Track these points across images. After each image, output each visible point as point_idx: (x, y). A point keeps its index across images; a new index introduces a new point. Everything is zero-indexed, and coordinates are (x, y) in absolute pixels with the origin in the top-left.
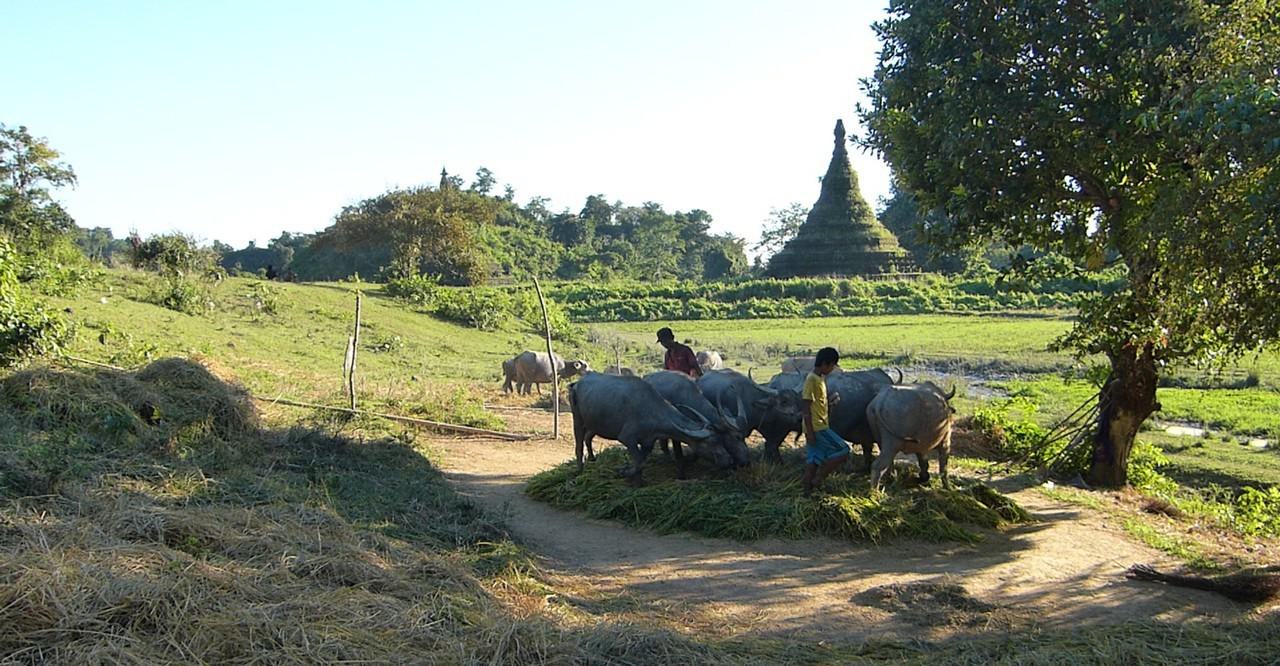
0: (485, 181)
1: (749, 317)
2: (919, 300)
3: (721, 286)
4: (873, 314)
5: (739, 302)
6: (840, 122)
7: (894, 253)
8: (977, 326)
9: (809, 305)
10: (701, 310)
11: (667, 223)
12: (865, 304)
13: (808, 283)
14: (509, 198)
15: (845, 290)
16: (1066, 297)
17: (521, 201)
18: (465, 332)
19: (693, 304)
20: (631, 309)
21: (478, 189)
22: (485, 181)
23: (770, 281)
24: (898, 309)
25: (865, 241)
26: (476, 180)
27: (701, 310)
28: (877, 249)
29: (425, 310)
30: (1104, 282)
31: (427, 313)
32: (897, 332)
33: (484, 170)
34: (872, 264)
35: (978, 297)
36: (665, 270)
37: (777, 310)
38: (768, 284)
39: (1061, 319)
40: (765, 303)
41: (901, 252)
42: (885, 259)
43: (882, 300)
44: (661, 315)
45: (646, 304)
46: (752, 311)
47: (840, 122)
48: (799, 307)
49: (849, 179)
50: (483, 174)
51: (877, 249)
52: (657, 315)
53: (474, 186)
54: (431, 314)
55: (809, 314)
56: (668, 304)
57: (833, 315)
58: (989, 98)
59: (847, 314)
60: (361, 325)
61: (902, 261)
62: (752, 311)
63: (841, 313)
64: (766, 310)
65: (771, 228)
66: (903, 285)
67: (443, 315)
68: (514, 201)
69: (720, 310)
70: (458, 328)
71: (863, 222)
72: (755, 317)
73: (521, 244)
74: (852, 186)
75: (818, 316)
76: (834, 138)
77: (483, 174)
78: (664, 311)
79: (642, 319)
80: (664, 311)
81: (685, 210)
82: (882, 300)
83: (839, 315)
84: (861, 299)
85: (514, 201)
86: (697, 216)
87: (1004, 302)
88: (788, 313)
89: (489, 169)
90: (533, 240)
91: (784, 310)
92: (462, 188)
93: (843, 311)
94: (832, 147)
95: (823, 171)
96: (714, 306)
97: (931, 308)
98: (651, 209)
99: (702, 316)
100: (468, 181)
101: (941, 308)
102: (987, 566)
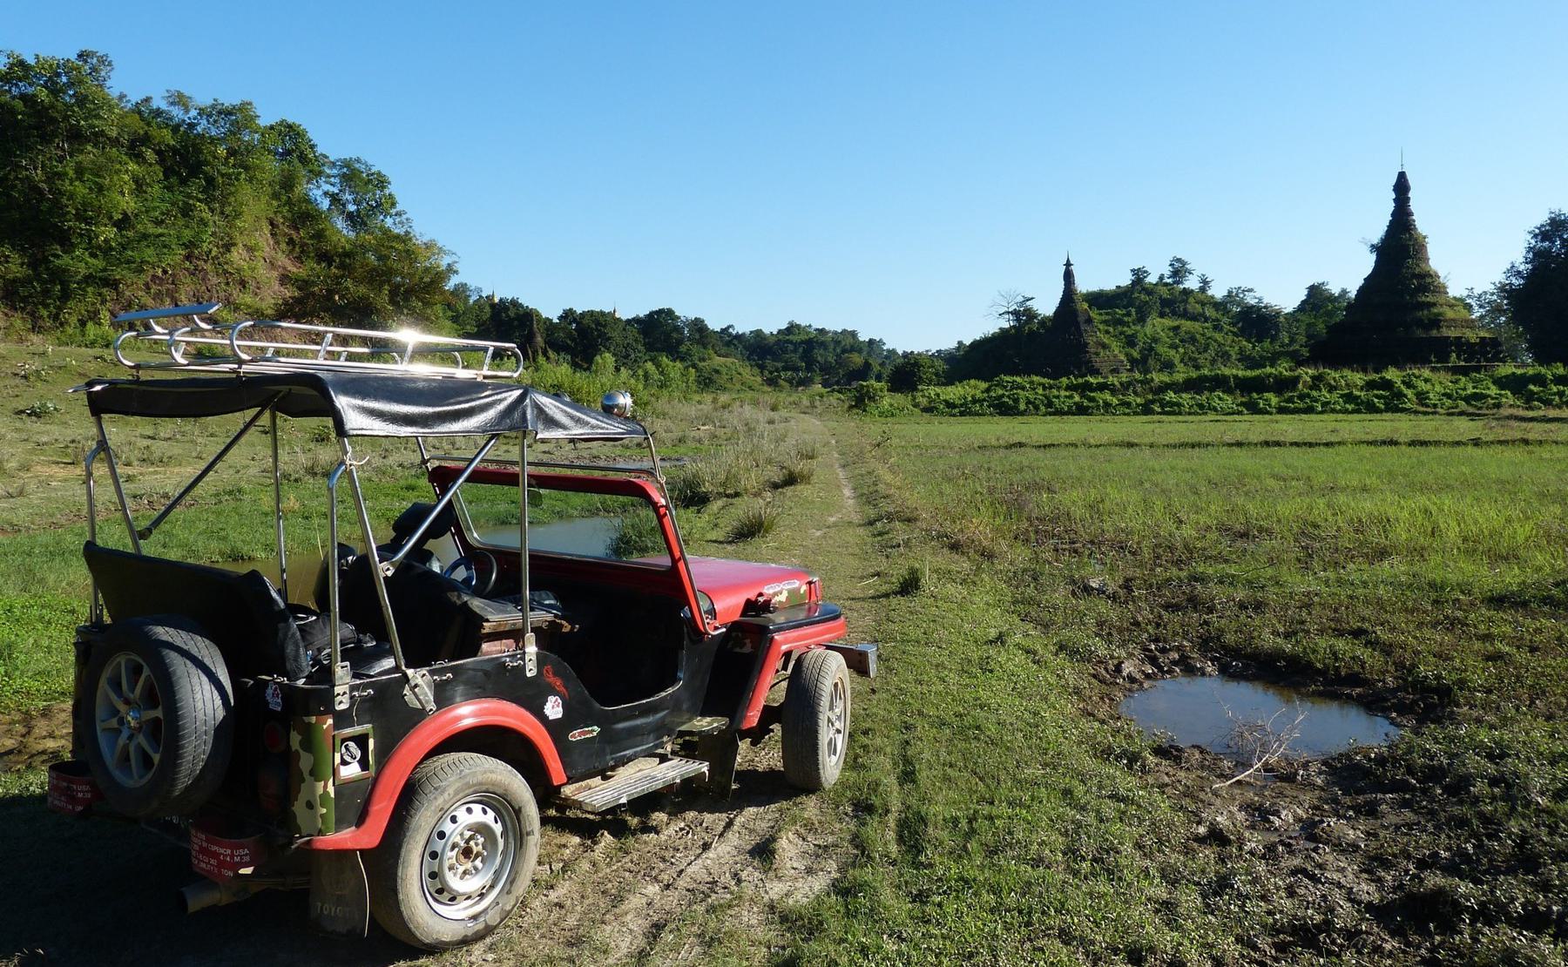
0: (1179, 270)
6: (1402, 177)
14: (1203, 290)
17: (1218, 291)
20: (1011, 402)
22: (1179, 270)
25: (1420, 323)
28: (1434, 333)
32: (553, 433)
33: (1179, 260)
47: (1402, 177)
50: (1177, 265)
51: (1434, 333)
58: (71, 93)
68: (1210, 293)
73: (1193, 340)
76: (1393, 196)
77: (1177, 265)
79: (1022, 413)
85: (1210, 293)
90: (1208, 335)
92: (1148, 280)
94: (1391, 206)
102: (820, 758)
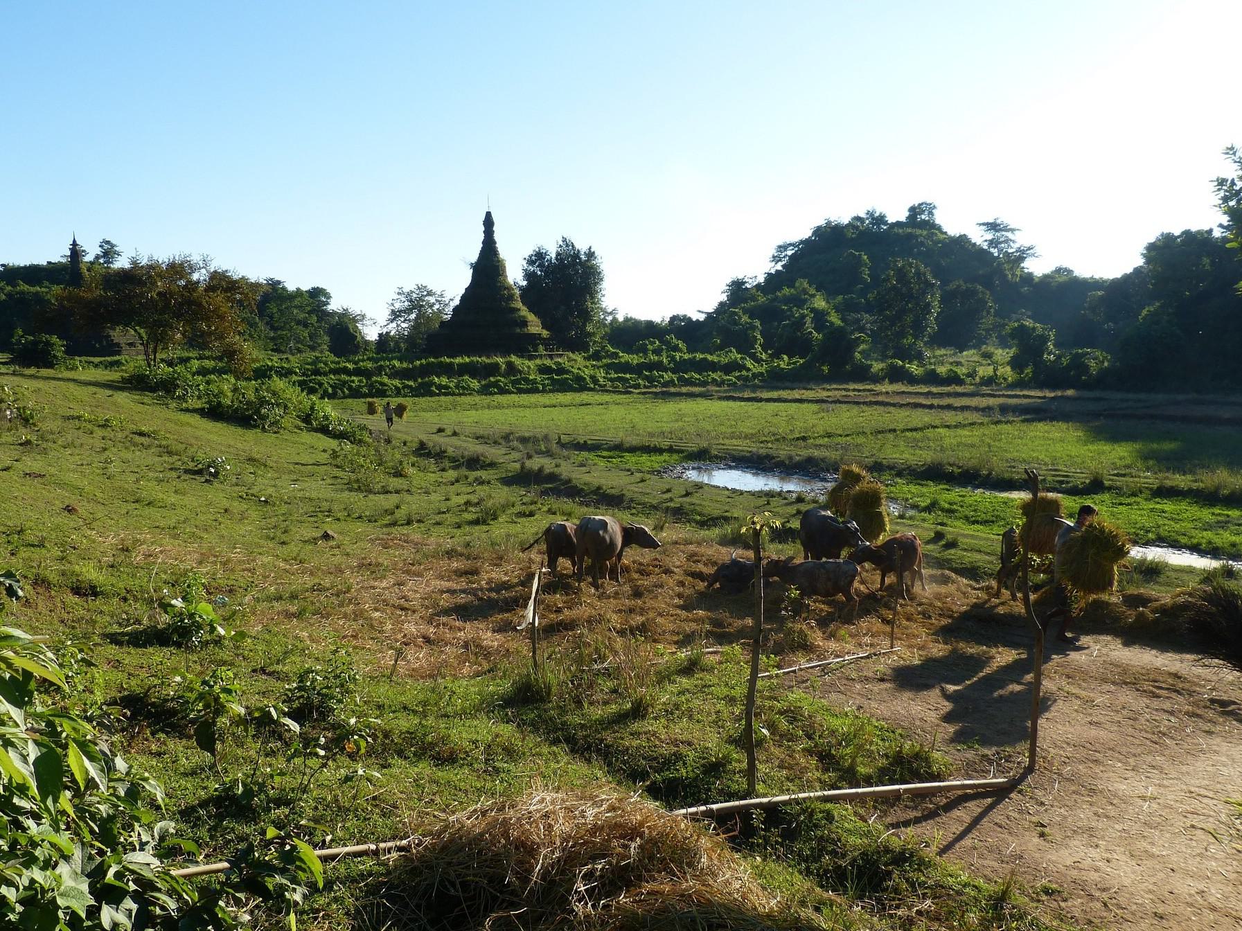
1: (432, 394)
2: (579, 379)
3: (397, 363)
4: (544, 391)
5: (420, 380)
6: (488, 215)
7: (540, 334)
8: (978, 432)
9: (483, 383)
10: (386, 388)
11: (299, 299)
12: (534, 382)
13: (478, 361)
15: (511, 368)
16: (698, 377)
18: (251, 435)
19: (376, 381)
21: (102, 261)
23: (443, 360)
24: (563, 387)
26: (99, 251)
27: (386, 388)
29: (191, 408)
30: (722, 363)
31: (195, 411)
33: (108, 242)
34: (525, 345)
35: (628, 376)
36: (298, 342)
37: (457, 387)
38: (441, 362)
39: (720, 398)
40: (444, 381)
41: (545, 333)
42: (534, 339)
43: (548, 379)
44: (347, 392)
45: (331, 382)
46: (434, 388)
47: (488, 215)
48: (475, 384)
49: (498, 266)
50: (106, 246)
52: (343, 392)
53: (97, 257)
54: (201, 412)
55: (485, 391)
56: (353, 381)
57: (510, 392)
59: (520, 391)
60: (892, 648)
61: (547, 342)
62: (434, 388)
63: (515, 390)
64: (447, 387)
65: (398, 306)
66: (560, 364)
67: (215, 413)
69: (403, 388)
70: (240, 430)
71: (513, 305)
72: (438, 395)
74: (501, 272)
75: (495, 393)
77: (106, 246)
78: (350, 388)
80: (350, 388)
81: (305, 287)
82: (548, 379)
83: (513, 393)
84: (531, 377)
86: (317, 293)
87: (650, 380)
88: (465, 391)
89: (114, 242)
91: (463, 388)
93: (517, 389)
94: (482, 237)
95: (474, 257)
96: (397, 382)
97: (592, 386)
98: (274, 285)
99: (388, 393)
100: (91, 252)
101: (600, 386)
